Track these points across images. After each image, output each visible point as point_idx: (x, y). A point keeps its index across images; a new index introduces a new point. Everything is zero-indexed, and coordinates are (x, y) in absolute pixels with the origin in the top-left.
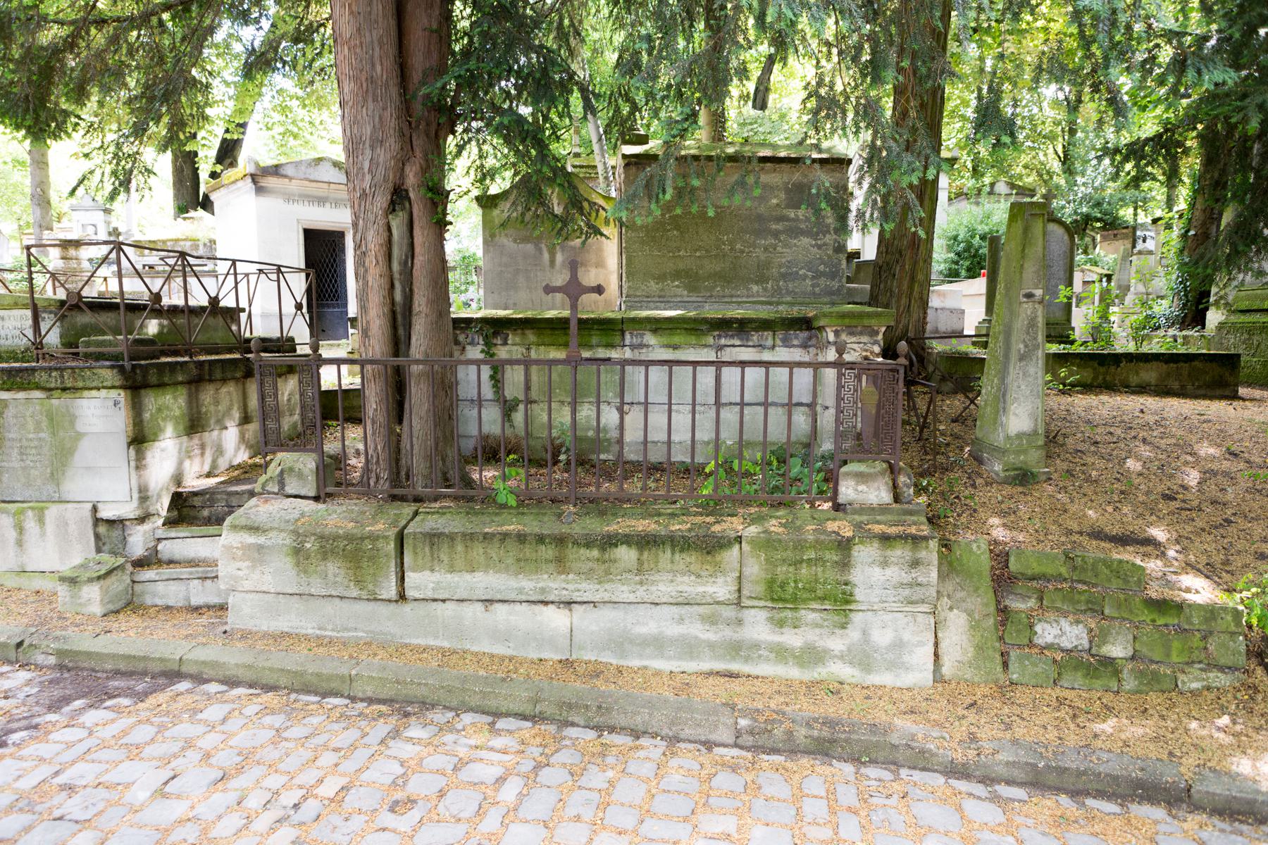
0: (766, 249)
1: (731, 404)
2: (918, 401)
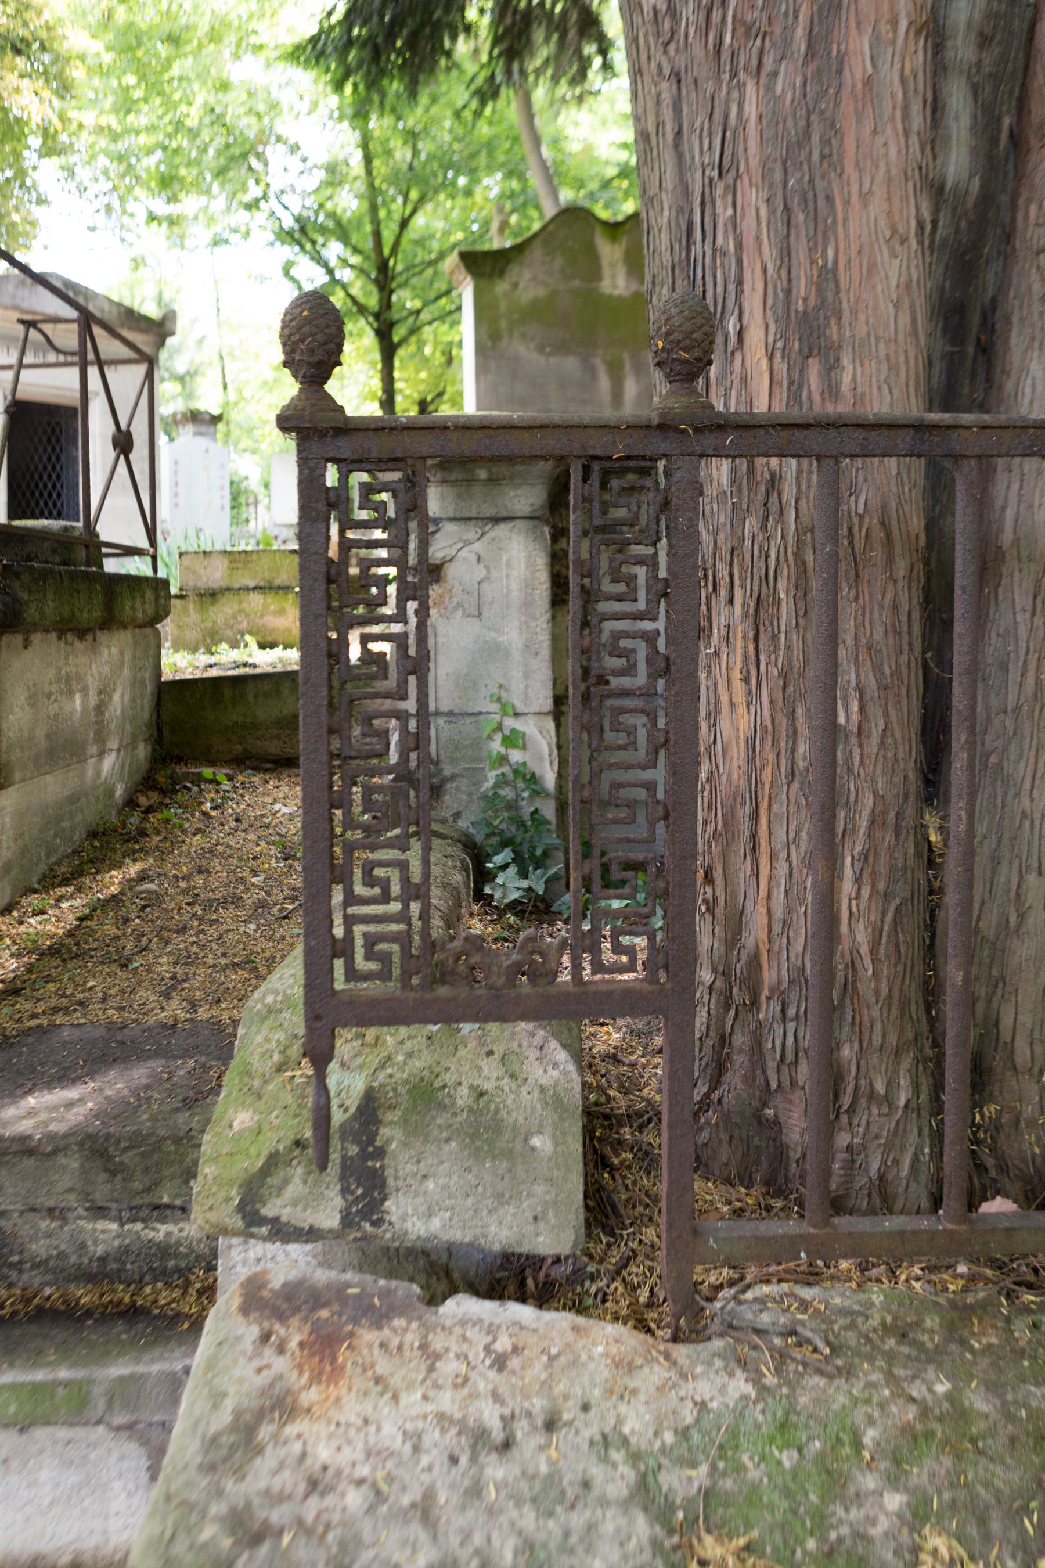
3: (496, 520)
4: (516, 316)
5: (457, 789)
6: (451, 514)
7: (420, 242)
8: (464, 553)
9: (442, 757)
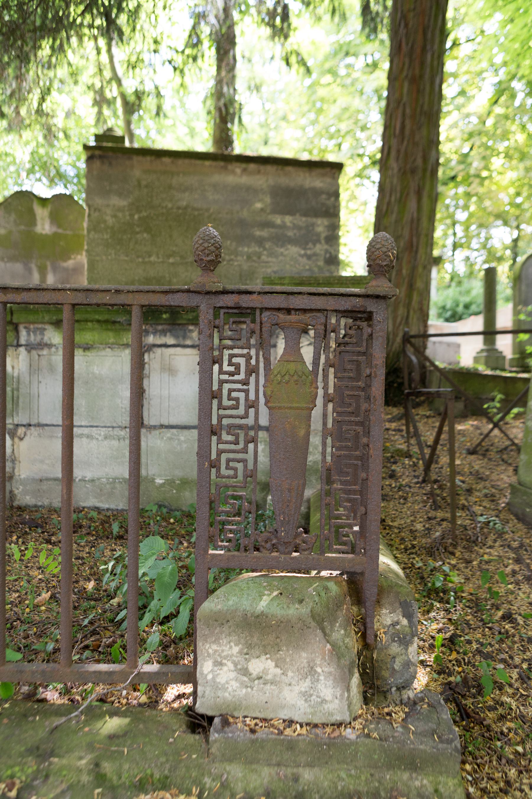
0: (249, 257)
1: (162, 426)
2: (421, 426)
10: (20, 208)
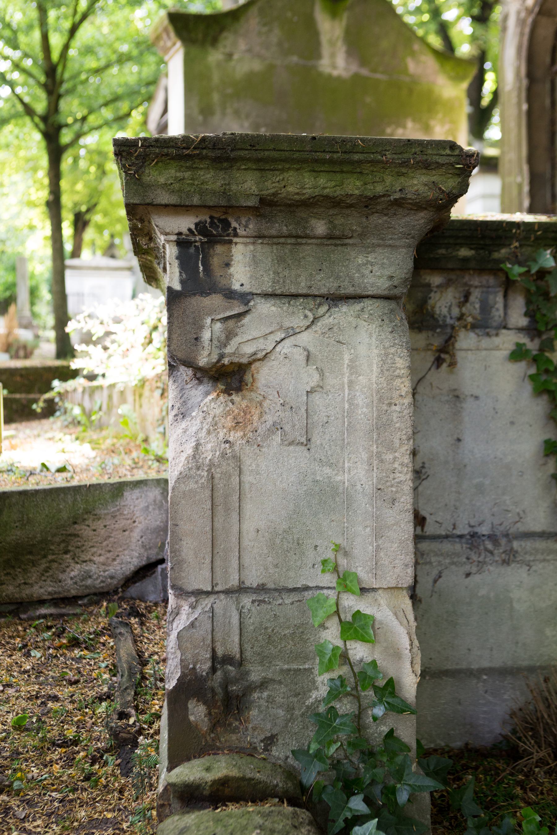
3: (336, 299)
4: (229, 91)
5: (270, 700)
6: (268, 288)
7: (88, 50)
8: (286, 347)
9: (248, 654)
10: (289, 14)
